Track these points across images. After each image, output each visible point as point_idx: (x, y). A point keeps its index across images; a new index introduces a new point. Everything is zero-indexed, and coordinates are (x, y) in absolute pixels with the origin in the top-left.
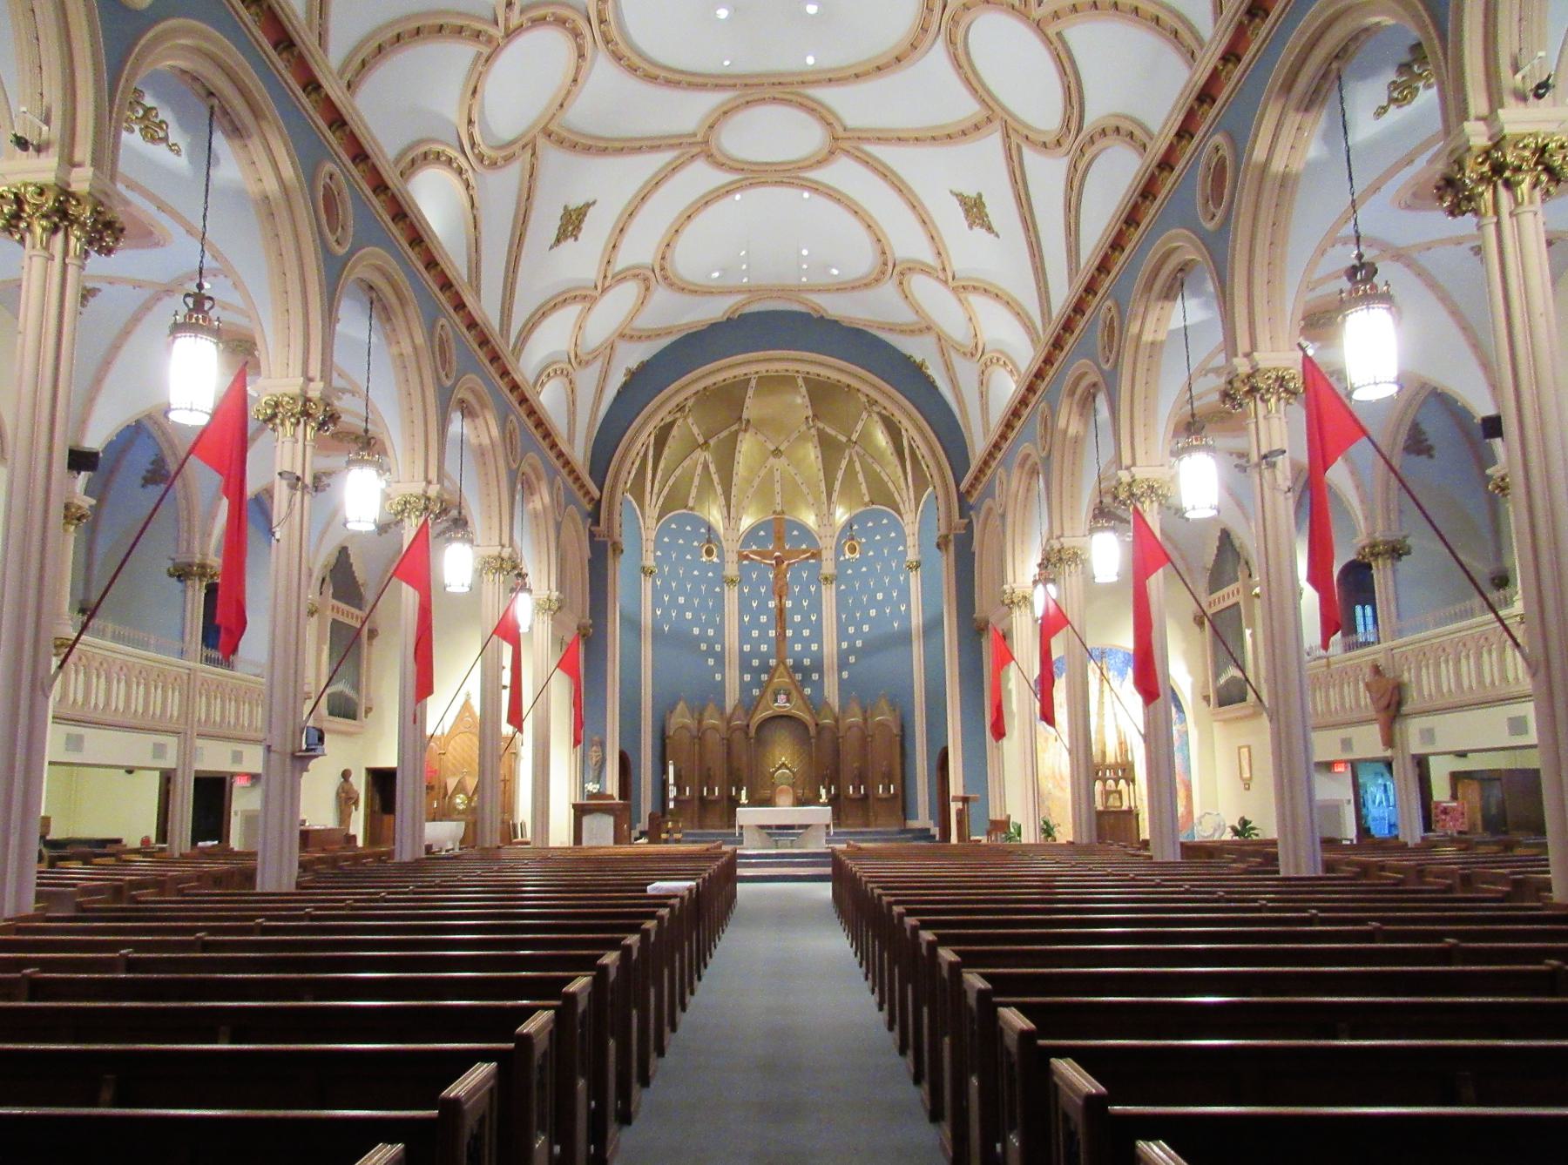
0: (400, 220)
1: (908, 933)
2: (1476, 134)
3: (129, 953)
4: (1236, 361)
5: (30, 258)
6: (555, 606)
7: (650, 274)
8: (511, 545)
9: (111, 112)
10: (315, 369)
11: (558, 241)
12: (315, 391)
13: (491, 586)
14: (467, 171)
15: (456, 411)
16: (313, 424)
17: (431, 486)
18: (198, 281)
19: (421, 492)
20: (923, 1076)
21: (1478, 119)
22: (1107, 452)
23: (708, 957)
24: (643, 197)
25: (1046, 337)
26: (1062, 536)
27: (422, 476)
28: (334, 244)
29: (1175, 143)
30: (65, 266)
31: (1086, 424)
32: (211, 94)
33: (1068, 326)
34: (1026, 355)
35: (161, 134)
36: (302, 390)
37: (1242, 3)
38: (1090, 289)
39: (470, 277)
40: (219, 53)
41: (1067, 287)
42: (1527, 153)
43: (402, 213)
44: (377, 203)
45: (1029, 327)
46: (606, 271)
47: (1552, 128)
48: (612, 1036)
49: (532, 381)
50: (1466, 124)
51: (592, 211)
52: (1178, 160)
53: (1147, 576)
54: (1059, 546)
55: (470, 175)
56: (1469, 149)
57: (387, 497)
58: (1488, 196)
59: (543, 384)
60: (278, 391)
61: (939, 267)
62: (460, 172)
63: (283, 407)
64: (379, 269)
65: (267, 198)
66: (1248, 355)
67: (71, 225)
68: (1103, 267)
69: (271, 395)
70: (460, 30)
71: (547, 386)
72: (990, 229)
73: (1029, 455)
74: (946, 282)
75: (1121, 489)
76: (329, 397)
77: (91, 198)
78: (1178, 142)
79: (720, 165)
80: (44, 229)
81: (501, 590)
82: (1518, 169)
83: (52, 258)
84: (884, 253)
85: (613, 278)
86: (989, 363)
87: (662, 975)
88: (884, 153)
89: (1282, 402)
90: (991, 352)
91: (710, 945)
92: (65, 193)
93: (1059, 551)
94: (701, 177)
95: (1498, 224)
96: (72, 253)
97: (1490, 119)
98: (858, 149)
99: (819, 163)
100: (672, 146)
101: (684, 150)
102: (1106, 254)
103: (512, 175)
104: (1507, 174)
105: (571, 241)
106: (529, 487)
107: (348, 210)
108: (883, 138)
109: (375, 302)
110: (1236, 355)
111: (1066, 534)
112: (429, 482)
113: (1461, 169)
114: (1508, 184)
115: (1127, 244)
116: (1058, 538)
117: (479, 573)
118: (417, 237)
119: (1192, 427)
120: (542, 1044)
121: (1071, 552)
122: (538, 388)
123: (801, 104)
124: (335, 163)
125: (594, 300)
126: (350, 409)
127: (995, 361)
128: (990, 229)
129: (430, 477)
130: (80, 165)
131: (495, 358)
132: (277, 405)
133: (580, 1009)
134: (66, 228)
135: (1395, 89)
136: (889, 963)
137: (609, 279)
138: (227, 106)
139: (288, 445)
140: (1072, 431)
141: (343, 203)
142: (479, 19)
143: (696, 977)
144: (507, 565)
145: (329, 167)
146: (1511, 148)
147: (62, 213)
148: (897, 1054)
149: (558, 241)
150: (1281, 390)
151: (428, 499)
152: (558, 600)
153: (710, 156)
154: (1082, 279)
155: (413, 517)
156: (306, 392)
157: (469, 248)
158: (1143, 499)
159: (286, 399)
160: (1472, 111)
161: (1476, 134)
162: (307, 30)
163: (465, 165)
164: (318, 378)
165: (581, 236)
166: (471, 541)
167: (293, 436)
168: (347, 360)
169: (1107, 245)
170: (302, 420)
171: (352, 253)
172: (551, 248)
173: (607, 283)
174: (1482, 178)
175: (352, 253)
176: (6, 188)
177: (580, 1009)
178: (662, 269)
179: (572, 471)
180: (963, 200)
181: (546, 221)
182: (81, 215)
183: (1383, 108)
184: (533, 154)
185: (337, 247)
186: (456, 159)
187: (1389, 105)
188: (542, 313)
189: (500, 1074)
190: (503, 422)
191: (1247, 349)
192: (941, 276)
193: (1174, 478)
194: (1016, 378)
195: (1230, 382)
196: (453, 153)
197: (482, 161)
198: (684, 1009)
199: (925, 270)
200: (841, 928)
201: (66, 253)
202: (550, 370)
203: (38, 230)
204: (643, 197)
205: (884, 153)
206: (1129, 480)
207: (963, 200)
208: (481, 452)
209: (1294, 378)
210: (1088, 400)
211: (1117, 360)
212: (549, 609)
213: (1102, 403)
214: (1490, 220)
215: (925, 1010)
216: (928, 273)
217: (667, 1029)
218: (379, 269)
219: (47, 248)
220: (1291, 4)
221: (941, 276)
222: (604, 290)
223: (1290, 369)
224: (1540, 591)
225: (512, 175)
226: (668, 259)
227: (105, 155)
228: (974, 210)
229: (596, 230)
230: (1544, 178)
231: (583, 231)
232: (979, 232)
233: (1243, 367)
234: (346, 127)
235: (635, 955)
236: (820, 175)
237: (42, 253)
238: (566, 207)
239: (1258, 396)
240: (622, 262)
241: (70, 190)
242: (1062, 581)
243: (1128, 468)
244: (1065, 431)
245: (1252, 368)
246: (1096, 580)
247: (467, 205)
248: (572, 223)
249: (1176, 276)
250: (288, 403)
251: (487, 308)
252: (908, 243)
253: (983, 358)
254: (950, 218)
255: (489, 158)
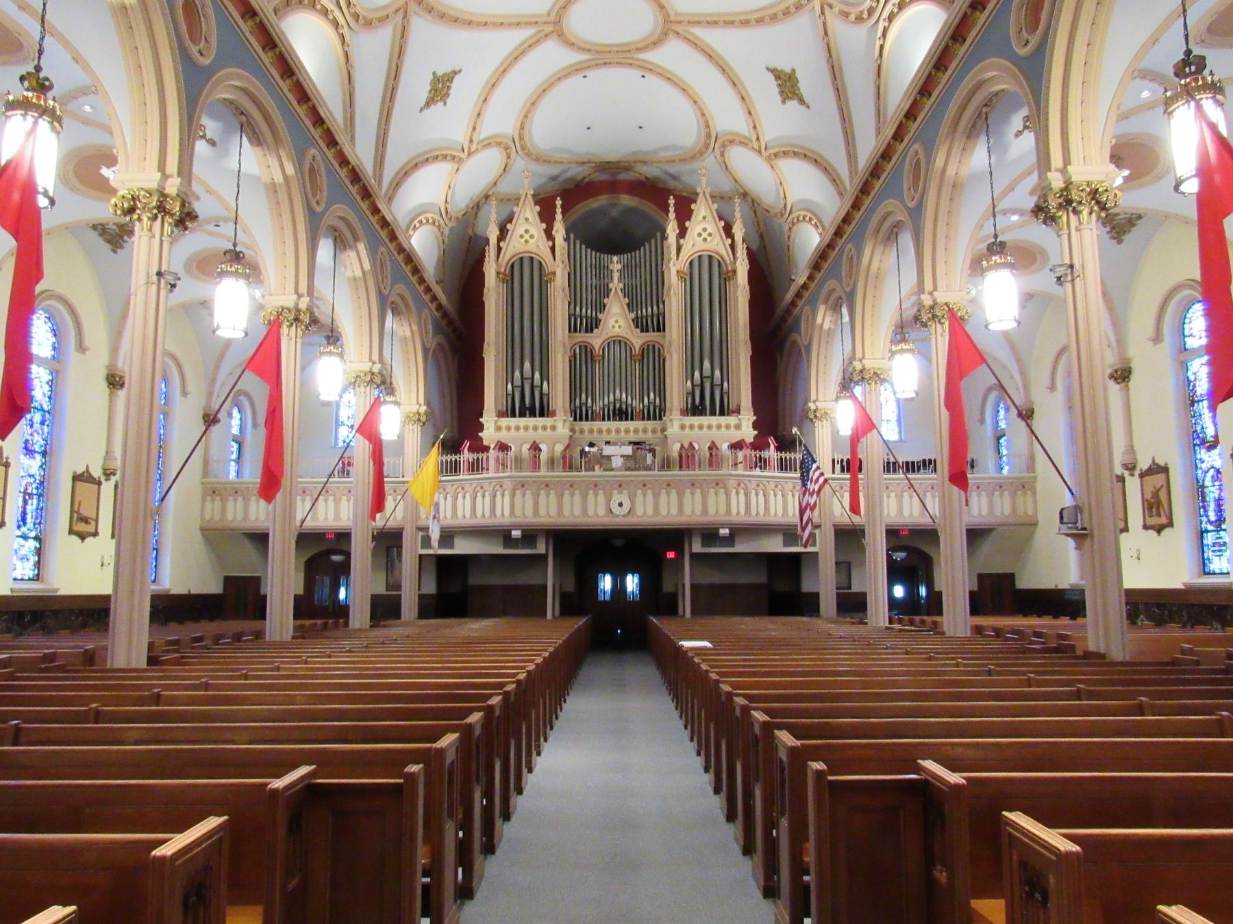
0: (288, 77)
1: (723, 698)
2: (1056, 181)
3: (97, 707)
4: (922, 297)
5: (140, 237)
6: (423, 418)
7: (511, 144)
8: (381, 360)
9: (189, 140)
10: (172, 165)
11: (428, 104)
12: (172, 187)
13: (411, 434)
14: (332, 11)
15: (326, 236)
16: (170, 220)
17: (302, 299)
18: (36, 63)
19: (369, 369)
20: (722, 789)
21: (1057, 170)
22: (910, 279)
23: (559, 710)
24: (504, 70)
25: (851, 187)
26: (817, 400)
27: (292, 290)
28: (315, 204)
29: (969, 13)
30: (162, 241)
31: (836, 322)
32: (242, 113)
33: (875, 172)
34: (831, 205)
35: (201, 134)
36: (159, 185)
37: (964, 2)
38: (898, 135)
39: (345, 125)
40: (252, 89)
41: (874, 136)
42: (1083, 194)
43: (269, 40)
44: (246, 27)
45: (835, 180)
46: (472, 135)
47: (1101, 177)
48: (498, 756)
49: (404, 225)
50: (1048, 174)
51: (457, 78)
52: (893, 155)
53: (962, 376)
54: (860, 367)
55: (346, 31)
56: (1051, 189)
57: (345, 373)
58: (1065, 218)
59: (415, 228)
60: (135, 186)
61: (754, 138)
62: (336, 25)
63: (140, 201)
64: (343, 219)
65: (125, 8)
66: (931, 293)
67: (165, 215)
68: (911, 114)
69: (128, 190)
70: (445, 157)
71: (419, 230)
72: (802, 101)
73: (834, 290)
74: (760, 152)
75: (855, 375)
76: (312, 308)
77: (179, 199)
78: (972, 13)
79: (571, 45)
80: (149, 218)
81: (299, 345)
82: (1080, 203)
83: (154, 236)
84: (708, 126)
85: (478, 143)
86: (795, 221)
87: (521, 728)
88: (710, 36)
89: (1094, 215)
90: (798, 211)
91: (551, 718)
92: (164, 196)
93: (861, 371)
94: (552, 56)
95: (1069, 234)
96: (165, 233)
97: (1063, 171)
98: (686, 31)
99: (656, 43)
100: (528, 24)
101: (540, 29)
102: (966, 14)
103: (383, 38)
104: (1074, 204)
105: (440, 104)
106: (342, 241)
107: (323, 179)
108: (712, 22)
109: (245, 125)
110: (924, 293)
111: (819, 399)
112: (300, 296)
113: (1046, 201)
114: (1075, 212)
115: (882, 173)
116: (814, 402)
117: (404, 424)
118: (287, 67)
119: (902, 332)
120: (450, 757)
121: (872, 372)
122: (411, 232)
123: (639, 66)
124: (316, 148)
125: (460, 161)
126: (323, 313)
127: (801, 218)
128: (802, 101)
129: (300, 291)
130: (171, 176)
131: (366, 194)
132: (133, 198)
133: (448, 761)
134: (163, 217)
135: (1027, 121)
136: (706, 720)
137: (475, 143)
138: (251, 120)
139: (145, 239)
140: (826, 326)
141: (208, 22)
142: (456, 150)
143: (548, 727)
144: (306, 319)
145: (313, 151)
146: (1075, 191)
147: (296, 319)
148: (712, 793)
149: (428, 104)
150: (1093, 202)
151: (373, 374)
152: (426, 413)
153: (561, 35)
154: (889, 132)
155: (362, 386)
156: (298, 305)
157: (344, 102)
158: (943, 321)
159: (142, 193)
160: (1053, 166)
161: (1056, 181)
162: (273, 14)
163: (341, 21)
164: (306, 295)
165: (448, 101)
166: (341, 355)
167: (150, 230)
168: (323, 284)
169: (916, 91)
170: (160, 216)
171: (326, 210)
172: (421, 110)
173: (474, 147)
174: (1060, 206)
175: (326, 210)
176: (127, 192)
177: (448, 761)
178: (521, 139)
179: (422, 281)
180: (777, 74)
181: (415, 85)
182: (173, 209)
183: (1020, 132)
184: (405, 16)
185: (201, 59)
186: (332, 11)
187: (1023, 130)
188: (415, 165)
189: (461, 739)
190: (372, 252)
191: (1060, 165)
192: (756, 146)
193: (890, 369)
194: (820, 230)
195: (919, 311)
196: (331, 6)
197: (357, 20)
198: (530, 770)
199: (744, 143)
200: (667, 692)
201: (162, 234)
202: (422, 217)
203: (145, 219)
204: (504, 70)
205: (710, 36)
206: (931, 303)
207: (777, 74)
208: (272, 188)
209: (1106, 190)
210: (836, 308)
211: (922, 198)
212: (419, 420)
213: (845, 310)
214: (1065, 231)
215: (712, 726)
216: (746, 145)
217: (525, 771)
218: (343, 219)
219: (150, 230)
220: (1000, 3)
221: (756, 146)
222: (470, 154)
223: (1103, 182)
224: (1087, 462)
225: (383, 38)
226: (526, 138)
227: (185, 170)
228: (788, 85)
229: (463, 93)
230: (1096, 208)
231: (451, 96)
232: (793, 104)
233: (1056, 181)
234: (257, 18)
235: (497, 712)
236: (652, 57)
237: (148, 233)
238: (434, 74)
239: (1070, 209)
240: (485, 131)
241: (165, 192)
242: (933, 340)
243: (814, 402)
244: (822, 326)
245: (1065, 182)
246: (840, 433)
247: (342, 59)
248: (440, 88)
249: (981, 111)
250: (145, 197)
251: (362, 153)
252: (728, 118)
253: (791, 217)
254: (765, 91)
255: (365, 18)
